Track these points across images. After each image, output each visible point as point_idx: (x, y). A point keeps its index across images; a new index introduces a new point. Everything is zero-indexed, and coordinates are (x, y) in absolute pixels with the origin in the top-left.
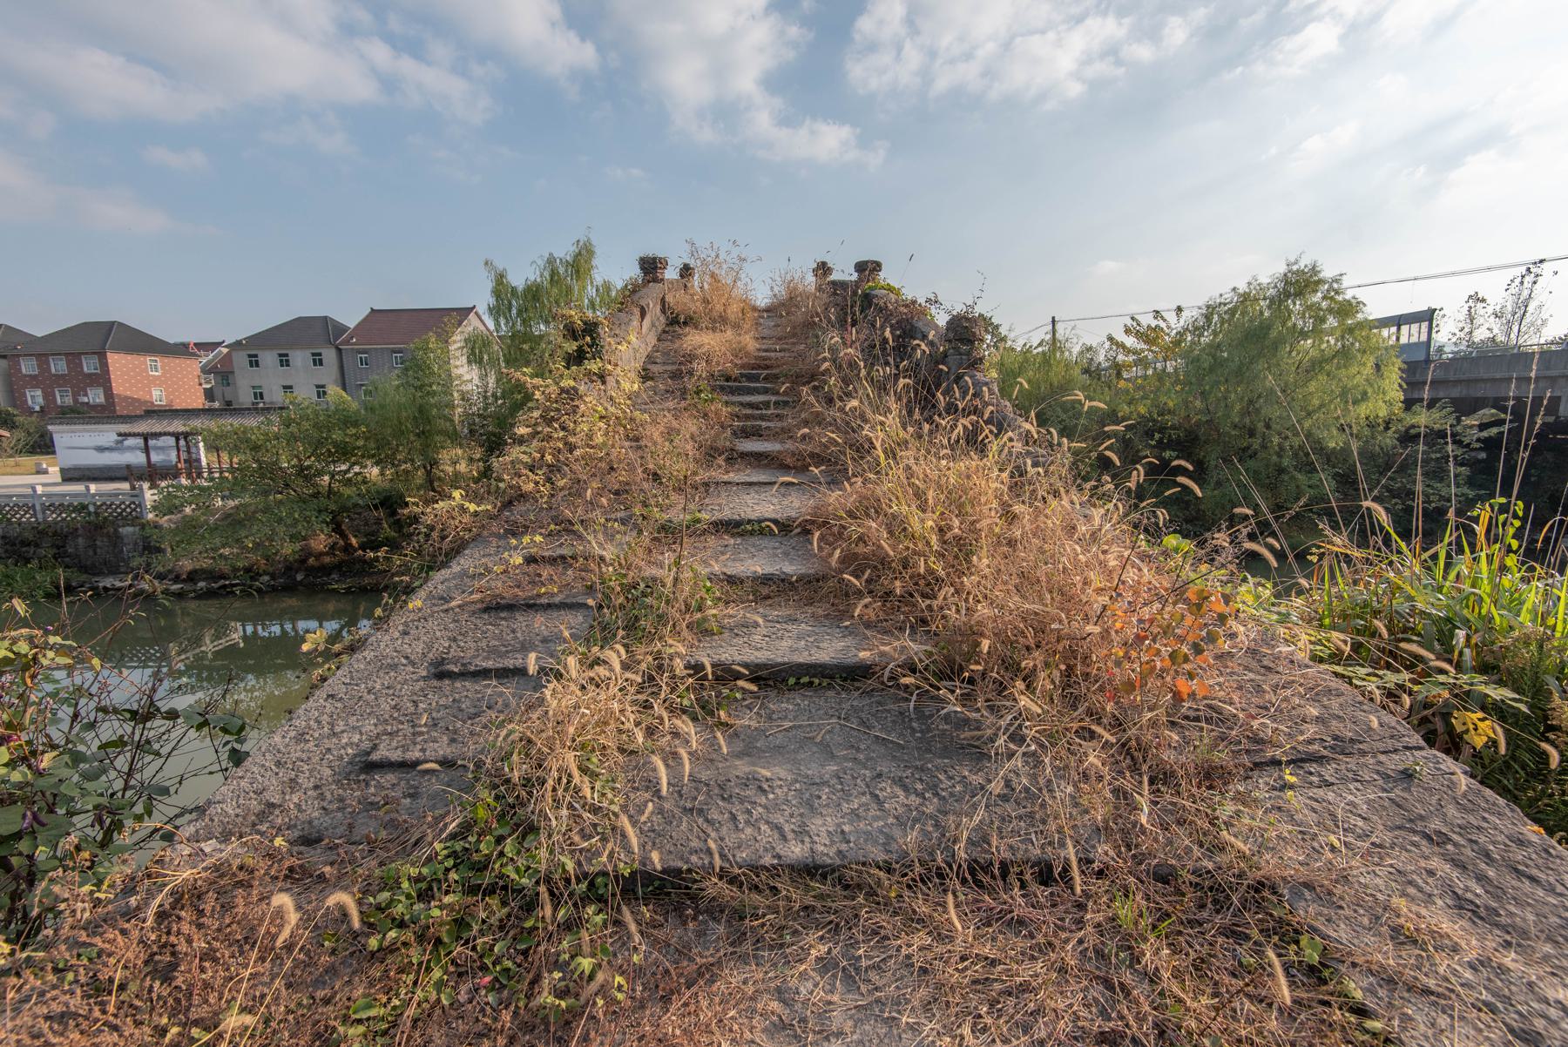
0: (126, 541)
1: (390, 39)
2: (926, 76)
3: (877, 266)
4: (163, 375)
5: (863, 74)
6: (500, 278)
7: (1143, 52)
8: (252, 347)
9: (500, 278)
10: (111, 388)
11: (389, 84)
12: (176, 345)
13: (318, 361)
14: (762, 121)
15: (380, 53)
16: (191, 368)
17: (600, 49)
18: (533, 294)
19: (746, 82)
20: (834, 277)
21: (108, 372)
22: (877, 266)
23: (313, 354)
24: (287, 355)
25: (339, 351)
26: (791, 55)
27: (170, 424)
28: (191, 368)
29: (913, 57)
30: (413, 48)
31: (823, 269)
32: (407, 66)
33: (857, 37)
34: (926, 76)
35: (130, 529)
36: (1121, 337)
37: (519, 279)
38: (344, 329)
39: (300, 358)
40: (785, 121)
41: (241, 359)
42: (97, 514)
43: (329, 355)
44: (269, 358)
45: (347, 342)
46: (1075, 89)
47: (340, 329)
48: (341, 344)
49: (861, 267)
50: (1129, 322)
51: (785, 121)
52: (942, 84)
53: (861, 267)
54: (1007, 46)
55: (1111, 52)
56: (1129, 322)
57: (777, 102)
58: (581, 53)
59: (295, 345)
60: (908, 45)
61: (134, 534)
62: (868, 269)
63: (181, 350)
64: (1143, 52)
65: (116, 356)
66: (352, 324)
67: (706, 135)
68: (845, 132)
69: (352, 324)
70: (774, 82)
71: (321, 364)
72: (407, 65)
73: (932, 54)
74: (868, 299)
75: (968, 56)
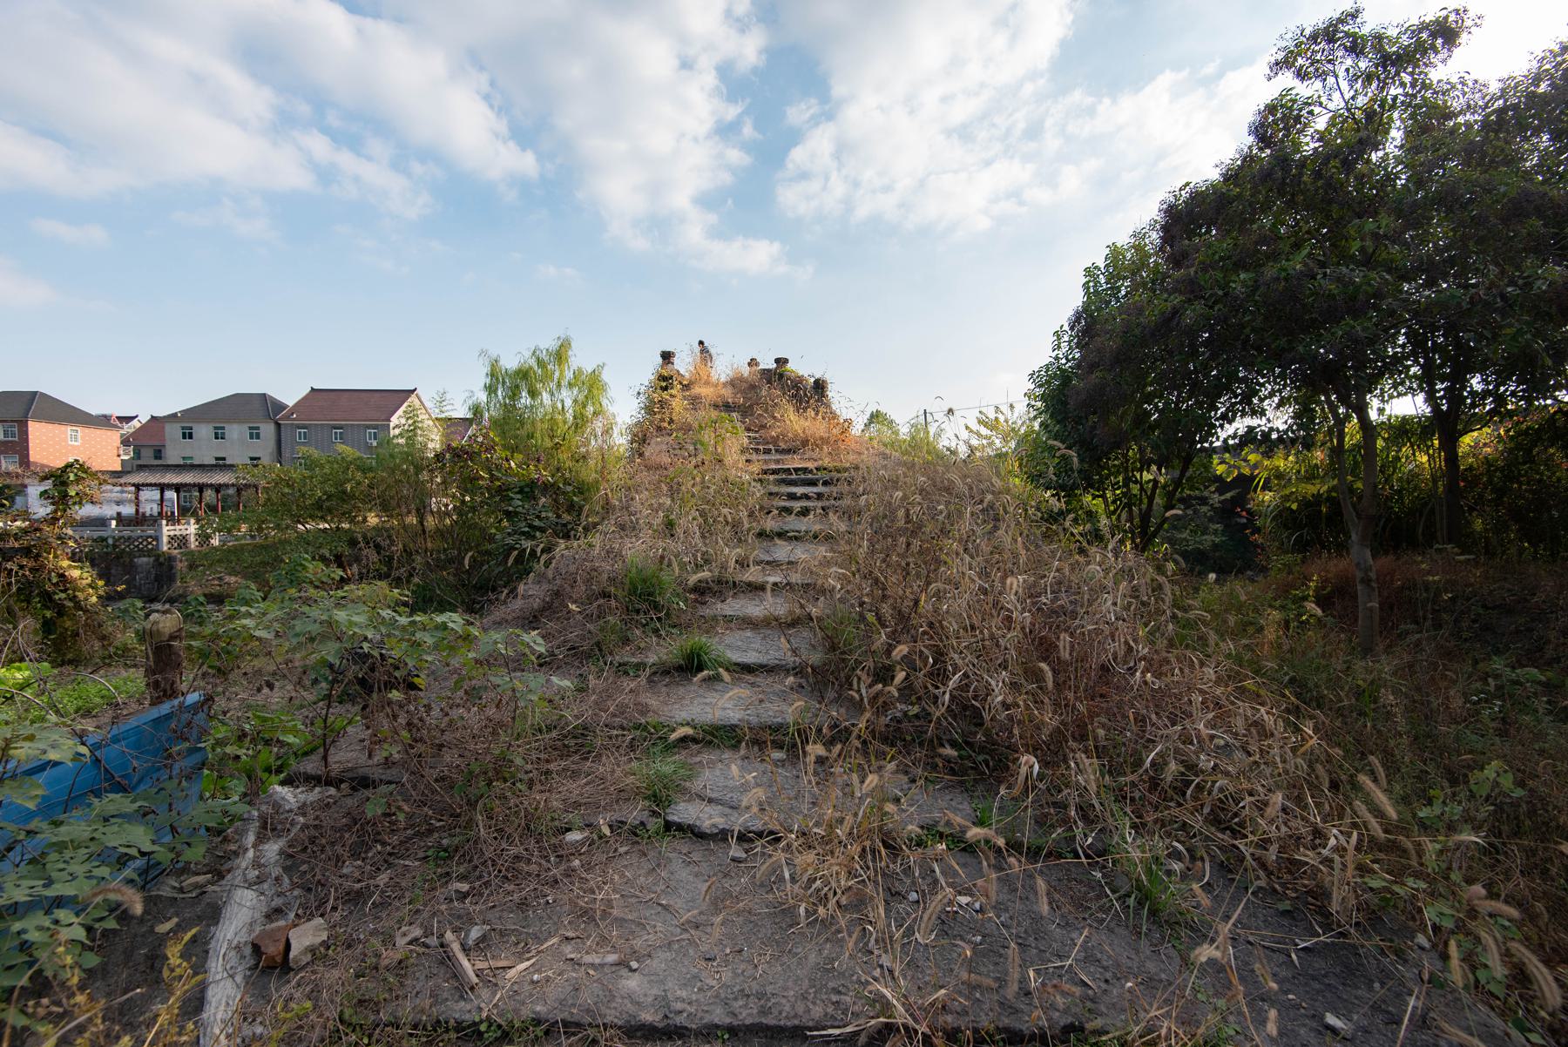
0: (139, 570)
1: (326, 131)
2: (848, 204)
3: (786, 361)
4: (82, 444)
5: (792, 198)
6: (494, 365)
7: (1042, 196)
8: (188, 420)
9: (494, 365)
10: (28, 455)
11: (326, 175)
12: (98, 417)
13: (255, 434)
14: (694, 233)
15: (319, 146)
16: (112, 438)
17: (540, 158)
18: (523, 374)
19: (681, 199)
20: (762, 366)
21: (27, 440)
22: (786, 361)
23: (250, 428)
24: (223, 428)
25: (278, 425)
26: (726, 178)
27: (162, 477)
28: (112, 438)
29: (838, 189)
30: (352, 143)
31: (753, 362)
32: (346, 160)
33: (790, 166)
34: (848, 204)
35: (145, 559)
36: (975, 426)
37: (510, 363)
38: (283, 407)
39: (235, 431)
40: (715, 233)
41: (173, 431)
42: (115, 546)
43: (268, 430)
44: (203, 431)
45: (288, 417)
46: (984, 223)
47: (280, 407)
48: (281, 419)
49: (778, 361)
50: (979, 415)
51: (715, 233)
52: (862, 212)
53: (778, 361)
54: (922, 184)
55: (1015, 194)
56: (979, 415)
57: (713, 218)
58: (527, 163)
59: (235, 419)
60: (834, 176)
61: (148, 564)
62: (781, 362)
63: (104, 421)
64: (1042, 196)
65: (37, 425)
66: (290, 402)
67: (640, 244)
68: (776, 247)
69: (290, 402)
70: (705, 201)
71: (258, 437)
72: (346, 160)
73: (856, 184)
74: (781, 376)
75: (887, 189)
